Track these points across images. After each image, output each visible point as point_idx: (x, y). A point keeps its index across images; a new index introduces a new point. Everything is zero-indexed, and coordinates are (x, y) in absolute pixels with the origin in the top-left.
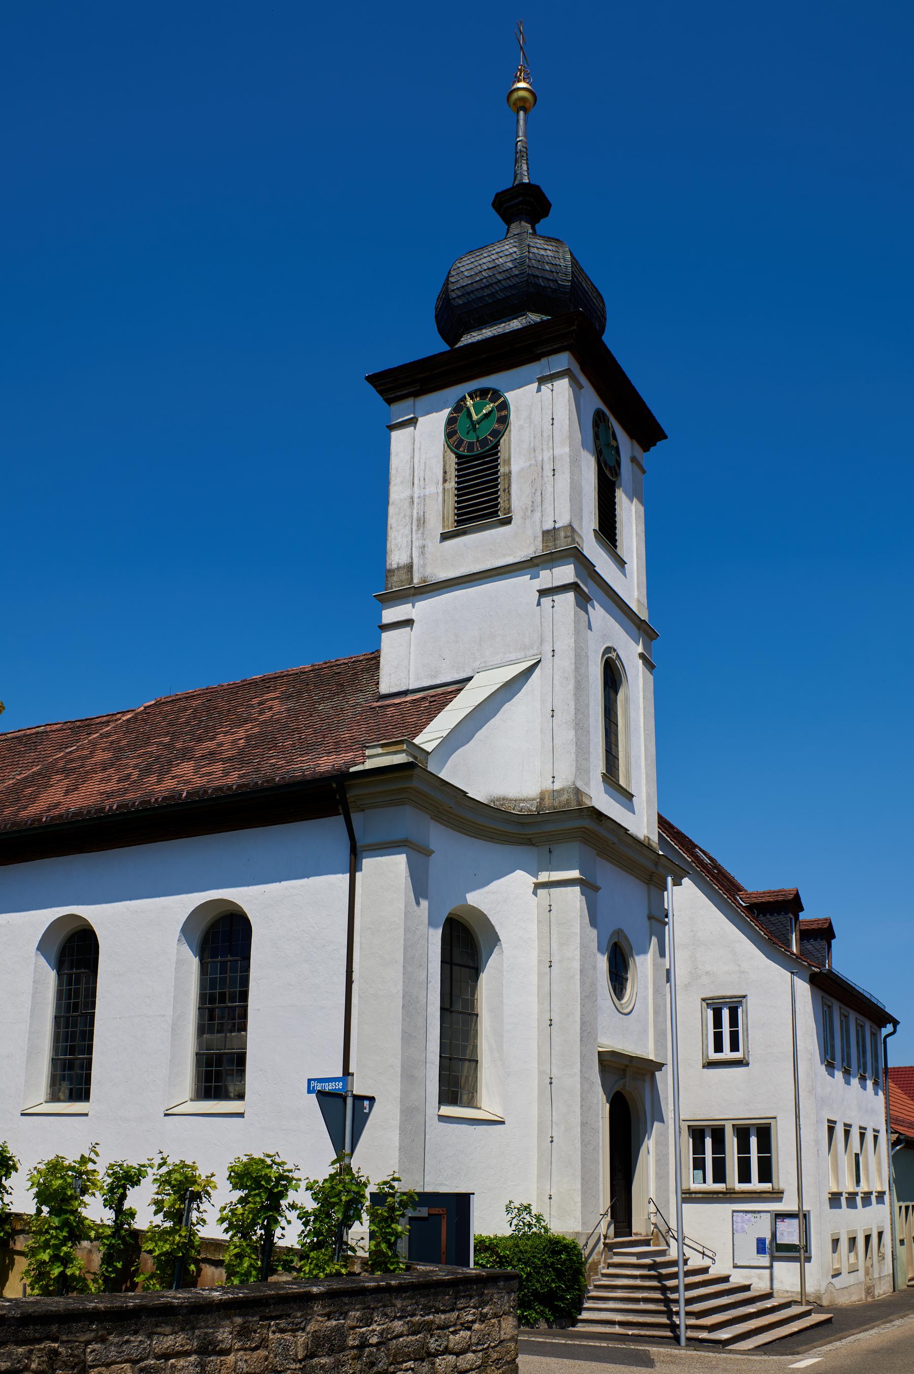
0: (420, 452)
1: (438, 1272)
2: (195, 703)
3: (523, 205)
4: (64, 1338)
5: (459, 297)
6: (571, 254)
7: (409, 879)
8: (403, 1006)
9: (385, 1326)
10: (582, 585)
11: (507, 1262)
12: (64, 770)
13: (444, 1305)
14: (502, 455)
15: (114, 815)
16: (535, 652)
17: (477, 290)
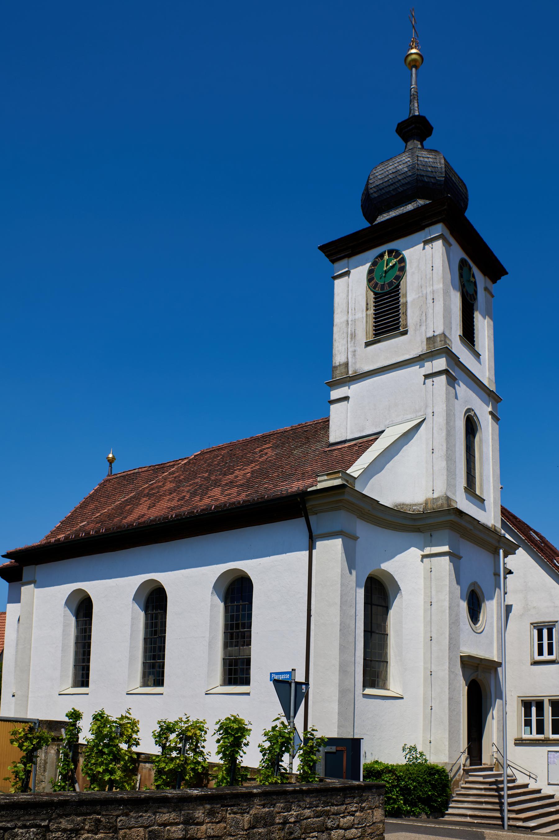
0: (352, 291)
1: (335, 782)
2: (223, 452)
3: (415, 129)
4: (104, 813)
5: (375, 192)
6: (445, 159)
7: (344, 555)
8: (340, 630)
9: (299, 812)
10: (451, 371)
11: (402, 779)
12: (148, 495)
13: (337, 801)
14: (402, 291)
15: (174, 521)
16: (422, 413)
17: (386, 187)
